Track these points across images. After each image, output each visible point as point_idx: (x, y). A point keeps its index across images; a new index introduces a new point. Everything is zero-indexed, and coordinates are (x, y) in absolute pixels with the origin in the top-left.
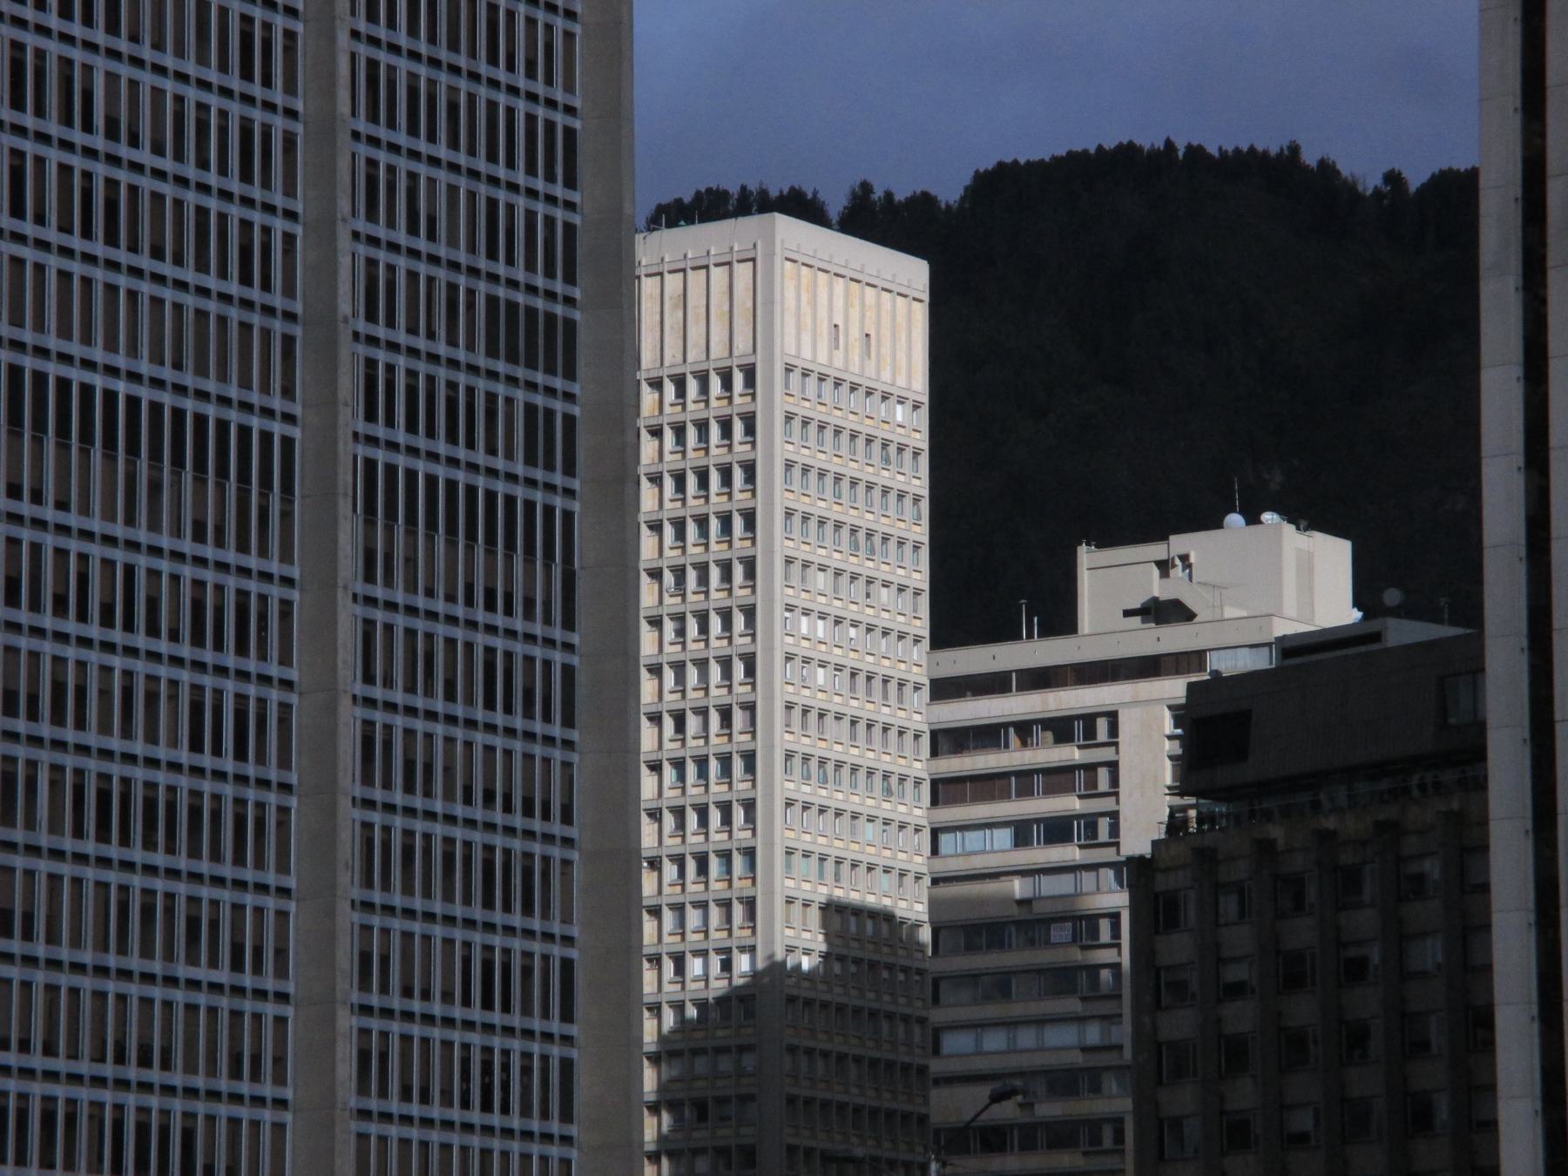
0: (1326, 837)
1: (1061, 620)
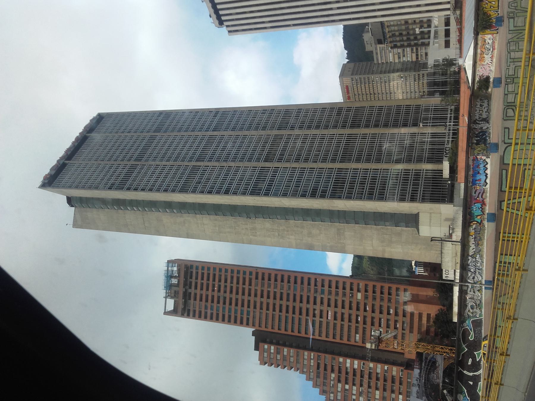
0: (388, 32)
1: (372, 52)
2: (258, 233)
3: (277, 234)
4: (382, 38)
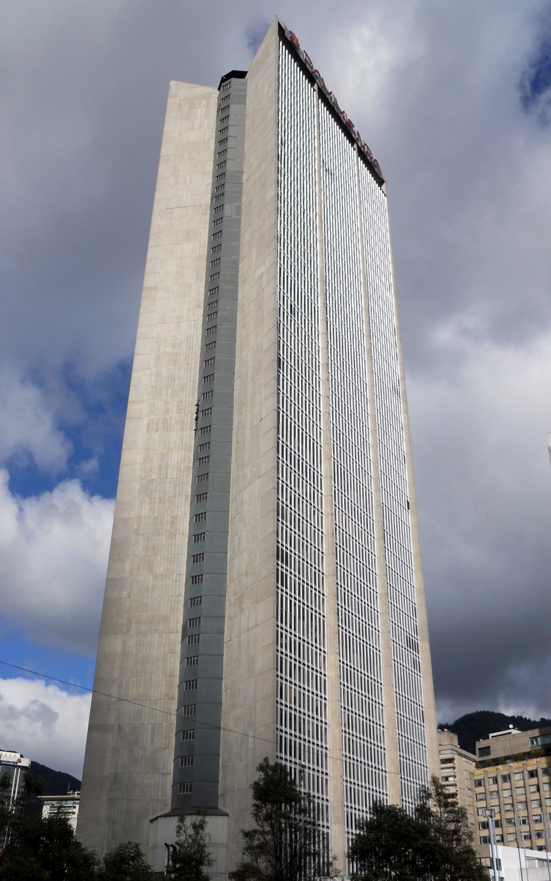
2: (156, 436)
3: (154, 476)
4: (492, 757)
